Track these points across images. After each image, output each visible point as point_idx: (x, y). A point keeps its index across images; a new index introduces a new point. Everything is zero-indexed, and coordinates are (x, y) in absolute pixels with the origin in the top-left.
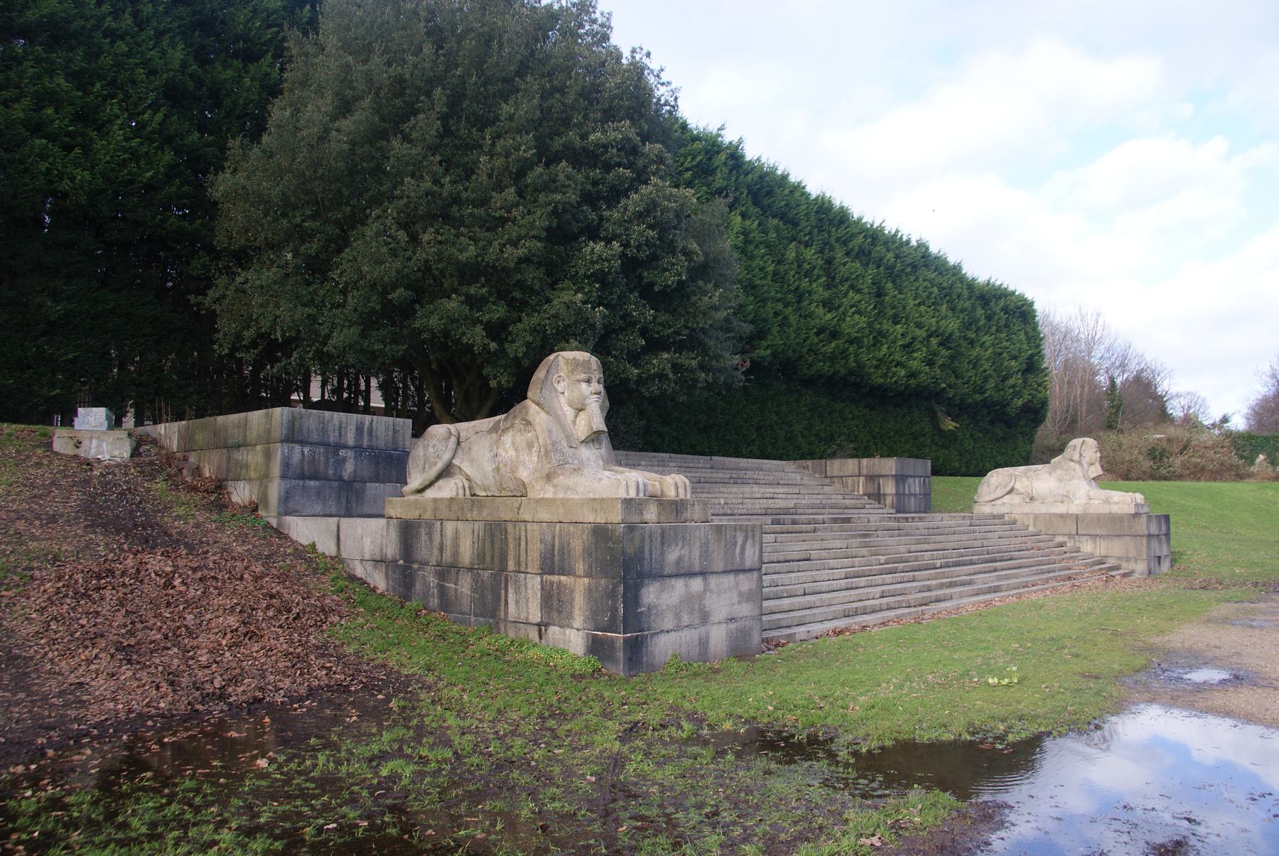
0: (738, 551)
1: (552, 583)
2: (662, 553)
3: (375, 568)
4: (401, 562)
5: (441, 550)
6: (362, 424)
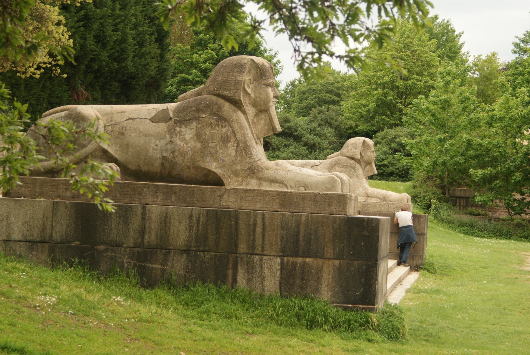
1: (294, 265)
5: (142, 231)
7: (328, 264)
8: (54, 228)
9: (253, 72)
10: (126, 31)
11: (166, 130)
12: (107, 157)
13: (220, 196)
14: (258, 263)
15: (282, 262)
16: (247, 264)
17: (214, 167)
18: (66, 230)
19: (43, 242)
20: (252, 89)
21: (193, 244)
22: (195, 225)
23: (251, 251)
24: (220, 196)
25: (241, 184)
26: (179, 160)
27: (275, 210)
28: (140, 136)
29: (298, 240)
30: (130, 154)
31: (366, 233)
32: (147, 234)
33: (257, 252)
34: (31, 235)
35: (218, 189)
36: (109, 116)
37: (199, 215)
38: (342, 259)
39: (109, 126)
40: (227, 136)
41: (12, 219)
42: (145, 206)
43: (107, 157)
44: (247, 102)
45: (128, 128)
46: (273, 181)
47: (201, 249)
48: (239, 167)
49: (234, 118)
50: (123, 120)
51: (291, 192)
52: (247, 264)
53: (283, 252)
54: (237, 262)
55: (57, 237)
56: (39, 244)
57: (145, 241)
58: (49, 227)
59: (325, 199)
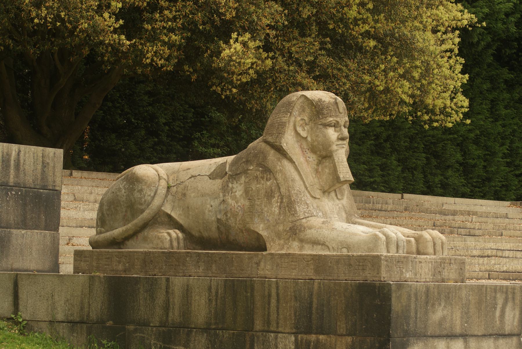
0: (498, 313)
1: (308, 343)
2: (426, 313)
3: (72, 330)
4: (110, 323)
5: (167, 308)
6: (9, 155)
7: (341, 341)
8: (91, 307)
9: (308, 110)
10: (431, 50)
11: (220, 187)
12: (172, 223)
13: (257, 263)
14: (274, 343)
15: (296, 340)
16: (263, 344)
17: (261, 229)
18: (101, 309)
19: (82, 322)
20: (308, 131)
21: (213, 321)
22: (214, 298)
23: (266, 328)
24: (257, 263)
25: (282, 249)
26: (231, 222)
27: (310, 277)
28: (198, 197)
29: (311, 313)
30: (191, 218)
31: (378, 302)
32: (171, 311)
33: (272, 329)
34: (72, 315)
35: (255, 255)
36: (175, 175)
37: (218, 286)
38: (355, 335)
39: (174, 186)
40: (271, 190)
41: (56, 297)
42: (169, 278)
43: (172, 223)
44: (305, 147)
45: (189, 188)
46: (315, 243)
47: (220, 326)
48: (281, 228)
49: (278, 168)
50: (187, 178)
51: (325, 256)
52: (263, 344)
53: (297, 328)
54: (254, 341)
55: (93, 316)
56: (78, 325)
57: (170, 319)
58: (86, 305)
59: (359, 262)
